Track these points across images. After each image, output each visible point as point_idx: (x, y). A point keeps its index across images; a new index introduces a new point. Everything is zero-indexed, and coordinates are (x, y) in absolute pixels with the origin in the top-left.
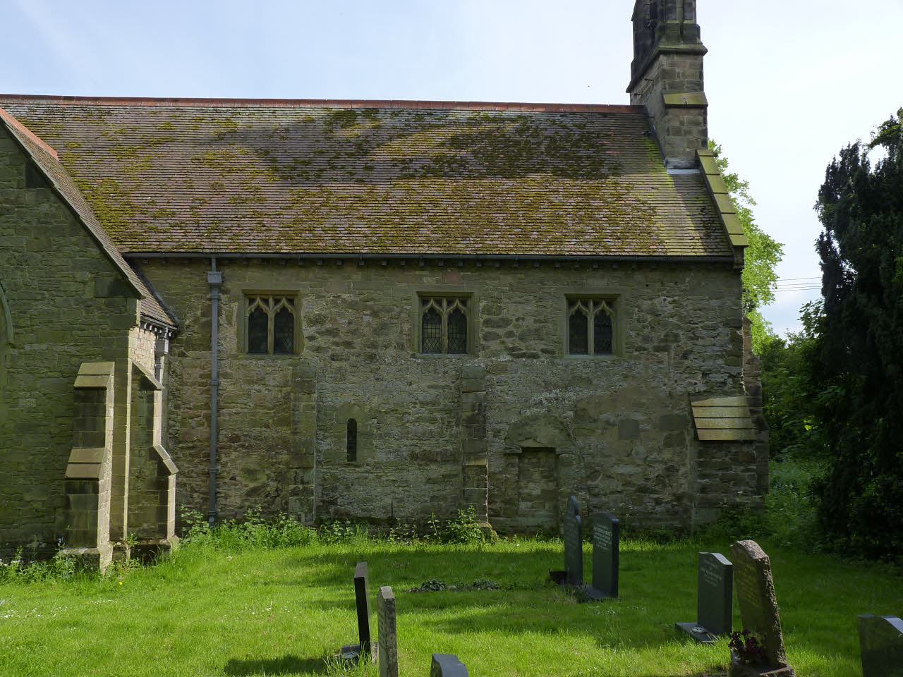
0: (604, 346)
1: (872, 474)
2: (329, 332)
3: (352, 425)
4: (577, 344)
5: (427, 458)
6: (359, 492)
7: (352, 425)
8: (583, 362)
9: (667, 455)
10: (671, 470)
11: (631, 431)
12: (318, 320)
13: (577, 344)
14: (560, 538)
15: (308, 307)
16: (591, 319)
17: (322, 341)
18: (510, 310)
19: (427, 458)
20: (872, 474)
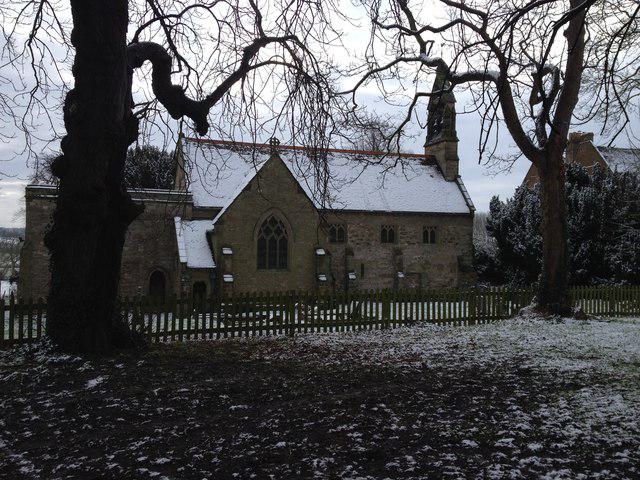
0: (433, 241)
1: (227, 251)
2: (356, 236)
3: (362, 265)
4: (425, 241)
5: (384, 276)
6: (364, 287)
7: (362, 265)
8: (428, 246)
9: (450, 275)
10: (452, 280)
11: (440, 267)
12: (352, 232)
13: (425, 241)
14: (484, 258)
15: (351, 228)
16: (495, 342)
17: (353, 239)
18: (408, 229)
19: (384, 276)
20: (227, 251)
